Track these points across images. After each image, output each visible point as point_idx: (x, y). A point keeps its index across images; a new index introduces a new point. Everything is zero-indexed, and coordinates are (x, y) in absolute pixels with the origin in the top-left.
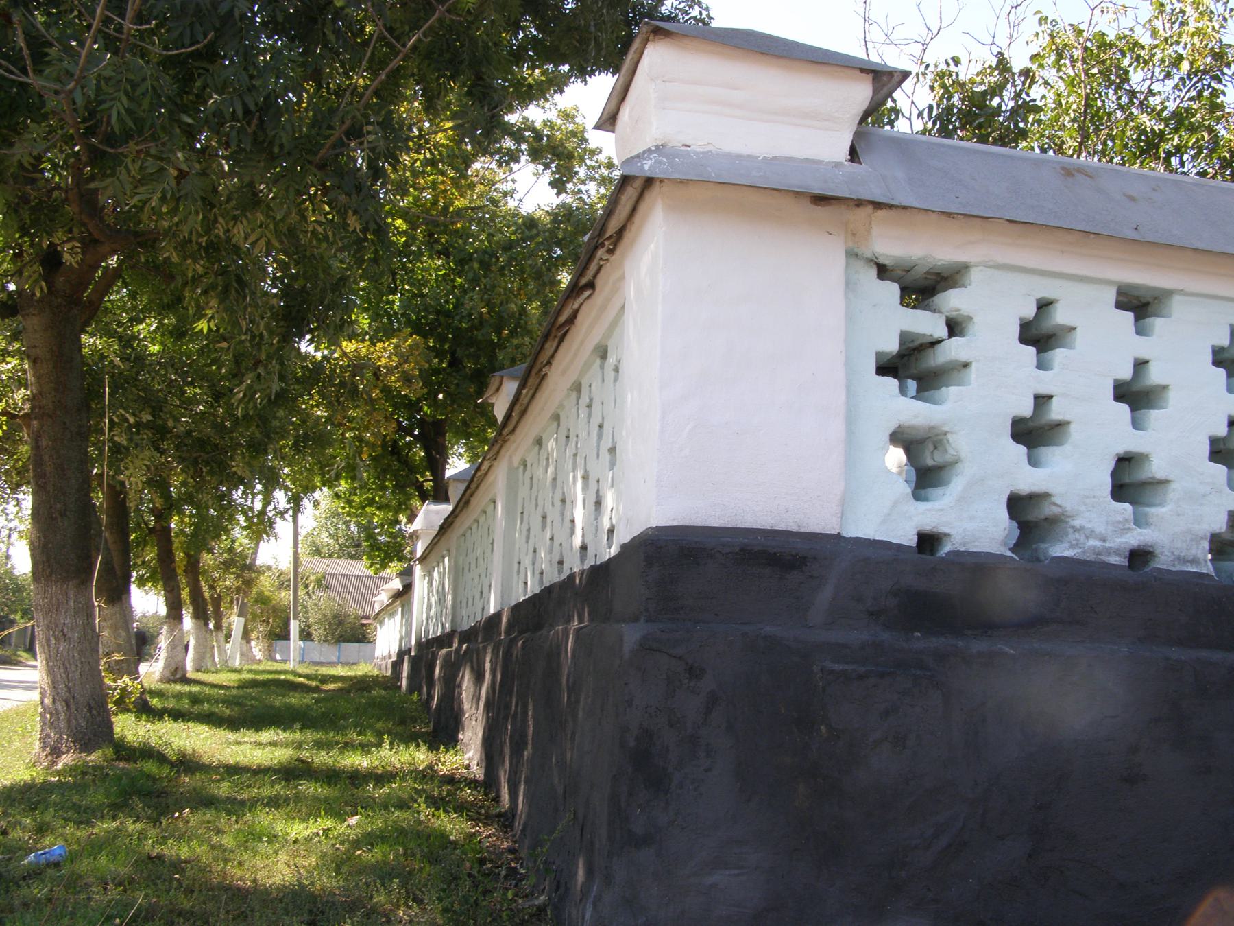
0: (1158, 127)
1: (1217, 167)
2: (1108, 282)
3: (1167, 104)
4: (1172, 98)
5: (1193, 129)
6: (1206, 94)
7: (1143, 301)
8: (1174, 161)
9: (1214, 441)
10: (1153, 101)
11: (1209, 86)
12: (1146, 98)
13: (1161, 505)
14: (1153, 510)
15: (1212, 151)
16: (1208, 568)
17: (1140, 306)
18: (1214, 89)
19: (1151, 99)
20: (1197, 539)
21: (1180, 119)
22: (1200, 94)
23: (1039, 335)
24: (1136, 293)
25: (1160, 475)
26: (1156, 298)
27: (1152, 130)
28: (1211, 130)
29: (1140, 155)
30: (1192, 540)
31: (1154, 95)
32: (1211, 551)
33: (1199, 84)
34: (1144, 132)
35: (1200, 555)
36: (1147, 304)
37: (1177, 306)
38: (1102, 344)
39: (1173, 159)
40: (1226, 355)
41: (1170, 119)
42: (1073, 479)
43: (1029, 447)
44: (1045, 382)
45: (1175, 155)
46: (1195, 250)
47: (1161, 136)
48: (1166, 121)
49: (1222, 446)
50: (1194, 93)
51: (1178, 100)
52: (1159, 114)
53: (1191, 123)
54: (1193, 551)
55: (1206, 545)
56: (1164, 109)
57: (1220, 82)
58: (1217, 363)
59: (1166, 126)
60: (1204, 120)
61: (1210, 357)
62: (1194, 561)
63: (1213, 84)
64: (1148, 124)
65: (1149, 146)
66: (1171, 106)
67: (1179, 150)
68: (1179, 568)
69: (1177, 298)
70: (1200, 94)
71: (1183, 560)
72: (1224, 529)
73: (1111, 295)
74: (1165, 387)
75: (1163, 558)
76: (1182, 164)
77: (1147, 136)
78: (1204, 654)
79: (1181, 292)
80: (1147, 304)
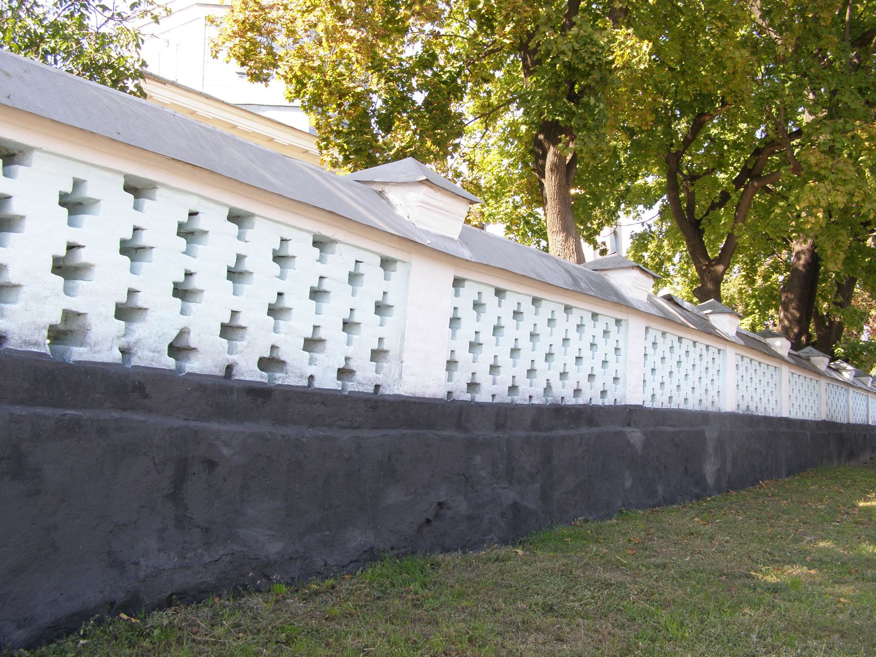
0: (40, 30)
1: (81, 69)
2: (227, 205)
3: (47, 15)
4: (52, 12)
5: (65, 38)
6: (77, 15)
7: (11, 152)
8: (50, 58)
9: (56, 259)
10: (37, 10)
11: (79, 10)
12: (32, 7)
13: (13, 302)
14: (238, 343)
15: (78, 57)
16: (46, 350)
17: (136, 189)
18: (82, 13)
19: (36, 9)
20: (39, 329)
21: (56, 29)
22: (72, 15)
23: (73, 205)
24: (5, 145)
25: (14, 280)
26: (21, 152)
27: (35, 32)
28: (78, 42)
29: (25, 49)
30: (35, 329)
31: (38, 6)
32: (49, 337)
33: (72, 8)
34: (29, 32)
35: (41, 340)
36: (13, 155)
37: (160, 193)
38: (114, 214)
39: (49, 57)
40: (69, 199)
41: (49, 27)
42: (203, 323)
43: (66, 279)
44: (191, 264)
45: (51, 54)
46: (52, 120)
47: (42, 38)
48: (46, 28)
49: (62, 263)
50: (68, 13)
51: (56, 15)
52: (41, 21)
53: (64, 34)
54: (36, 337)
55: (46, 333)
56: (45, 19)
57: (87, 9)
58: (62, 204)
59: (46, 31)
60: (74, 34)
61: (57, 199)
62: (36, 344)
63: (82, 10)
64: (33, 27)
65: (33, 43)
66: (51, 18)
67: (54, 51)
68: (24, 349)
69: (36, 154)
70: (72, 15)
71: (29, 343)
72: (59, 322)
73: (226, 213)
74: (23, 217)
75: (13, 341)
76: (56, 62)
77: (31, 36)
78: (39, 410)
79: (40, 150)
80: (13, 155)
